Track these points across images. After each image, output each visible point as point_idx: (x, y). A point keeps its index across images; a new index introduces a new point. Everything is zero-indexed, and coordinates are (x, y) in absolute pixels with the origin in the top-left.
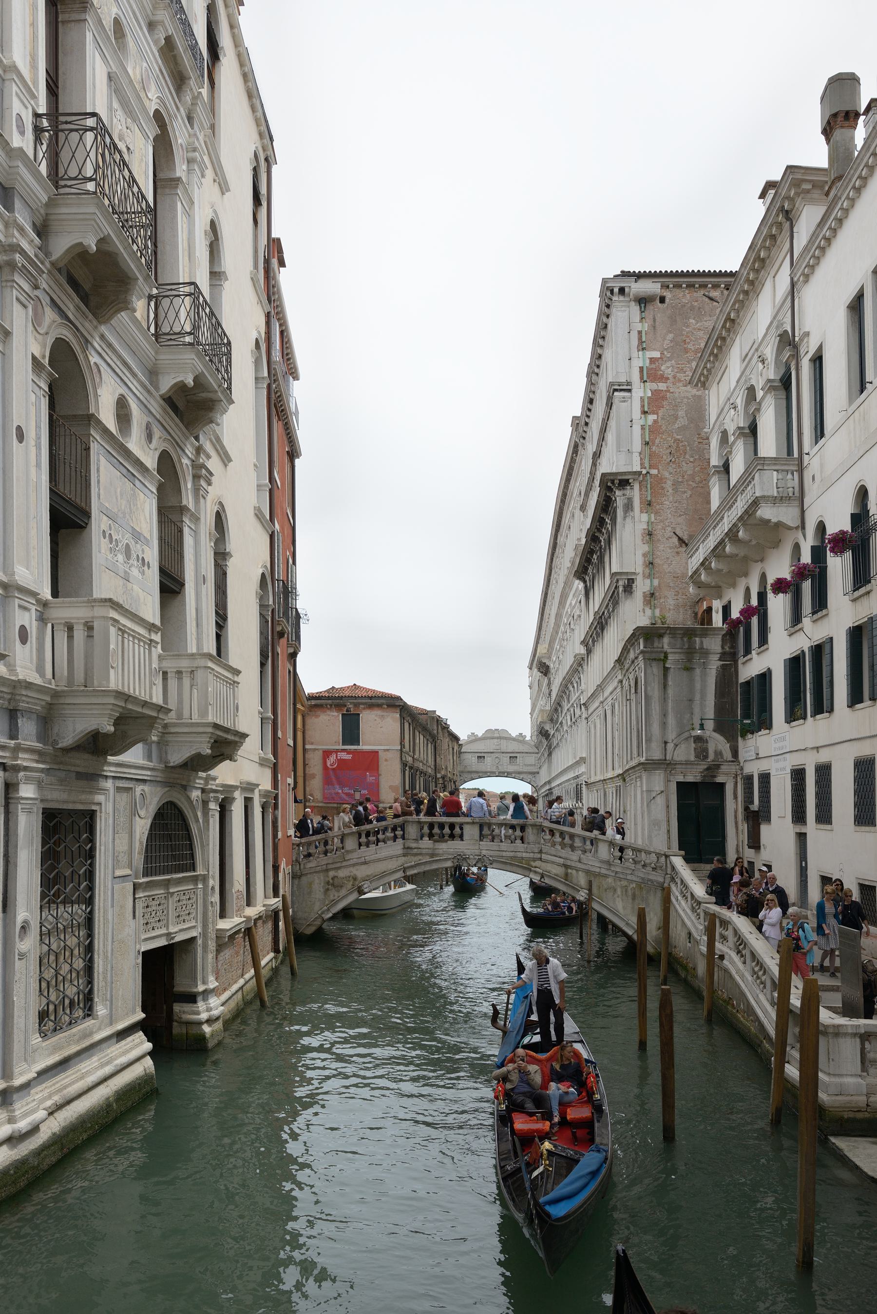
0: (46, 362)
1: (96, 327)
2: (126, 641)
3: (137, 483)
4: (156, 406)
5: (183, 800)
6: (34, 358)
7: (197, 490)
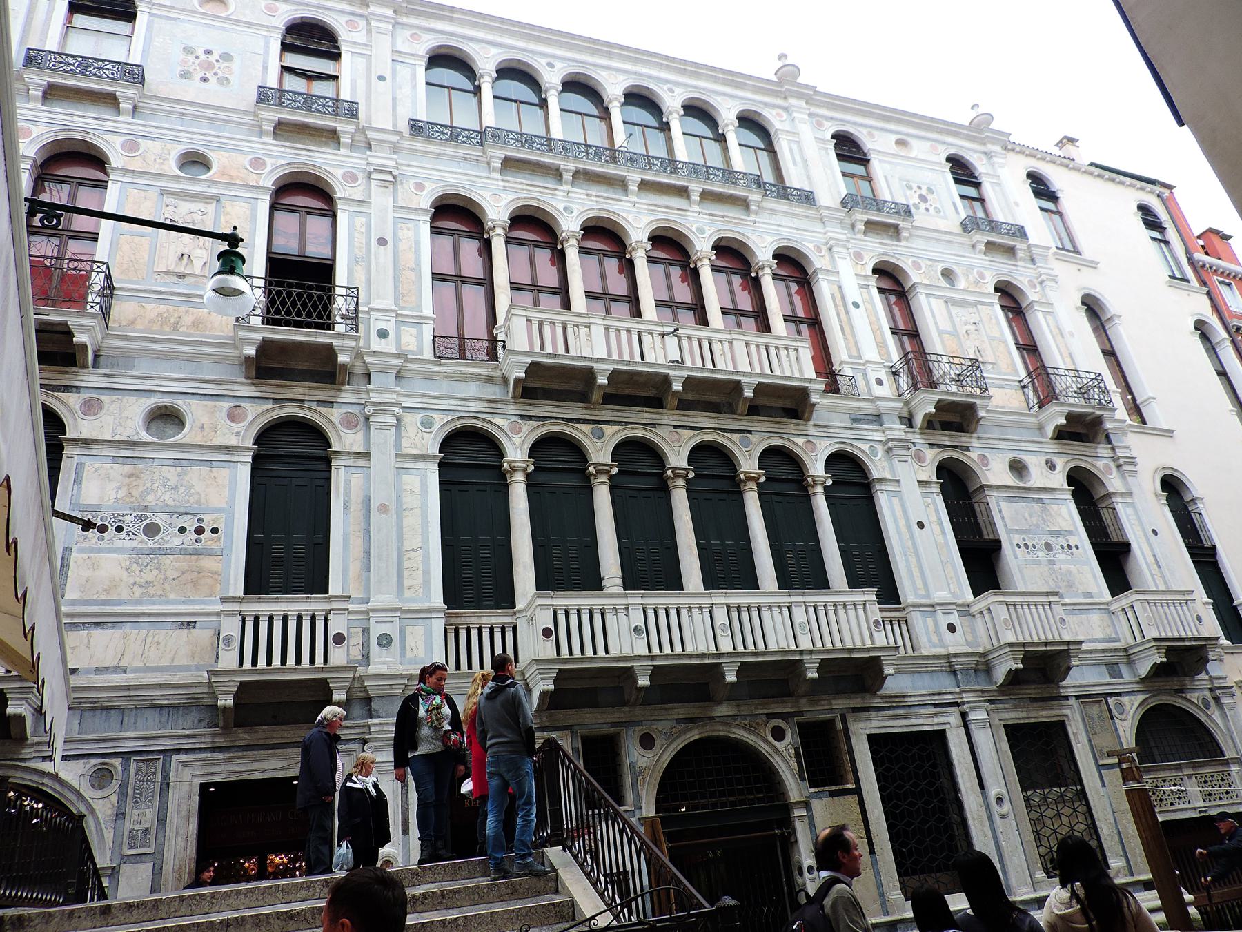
0: (935, 479)
4: (1052, 447)
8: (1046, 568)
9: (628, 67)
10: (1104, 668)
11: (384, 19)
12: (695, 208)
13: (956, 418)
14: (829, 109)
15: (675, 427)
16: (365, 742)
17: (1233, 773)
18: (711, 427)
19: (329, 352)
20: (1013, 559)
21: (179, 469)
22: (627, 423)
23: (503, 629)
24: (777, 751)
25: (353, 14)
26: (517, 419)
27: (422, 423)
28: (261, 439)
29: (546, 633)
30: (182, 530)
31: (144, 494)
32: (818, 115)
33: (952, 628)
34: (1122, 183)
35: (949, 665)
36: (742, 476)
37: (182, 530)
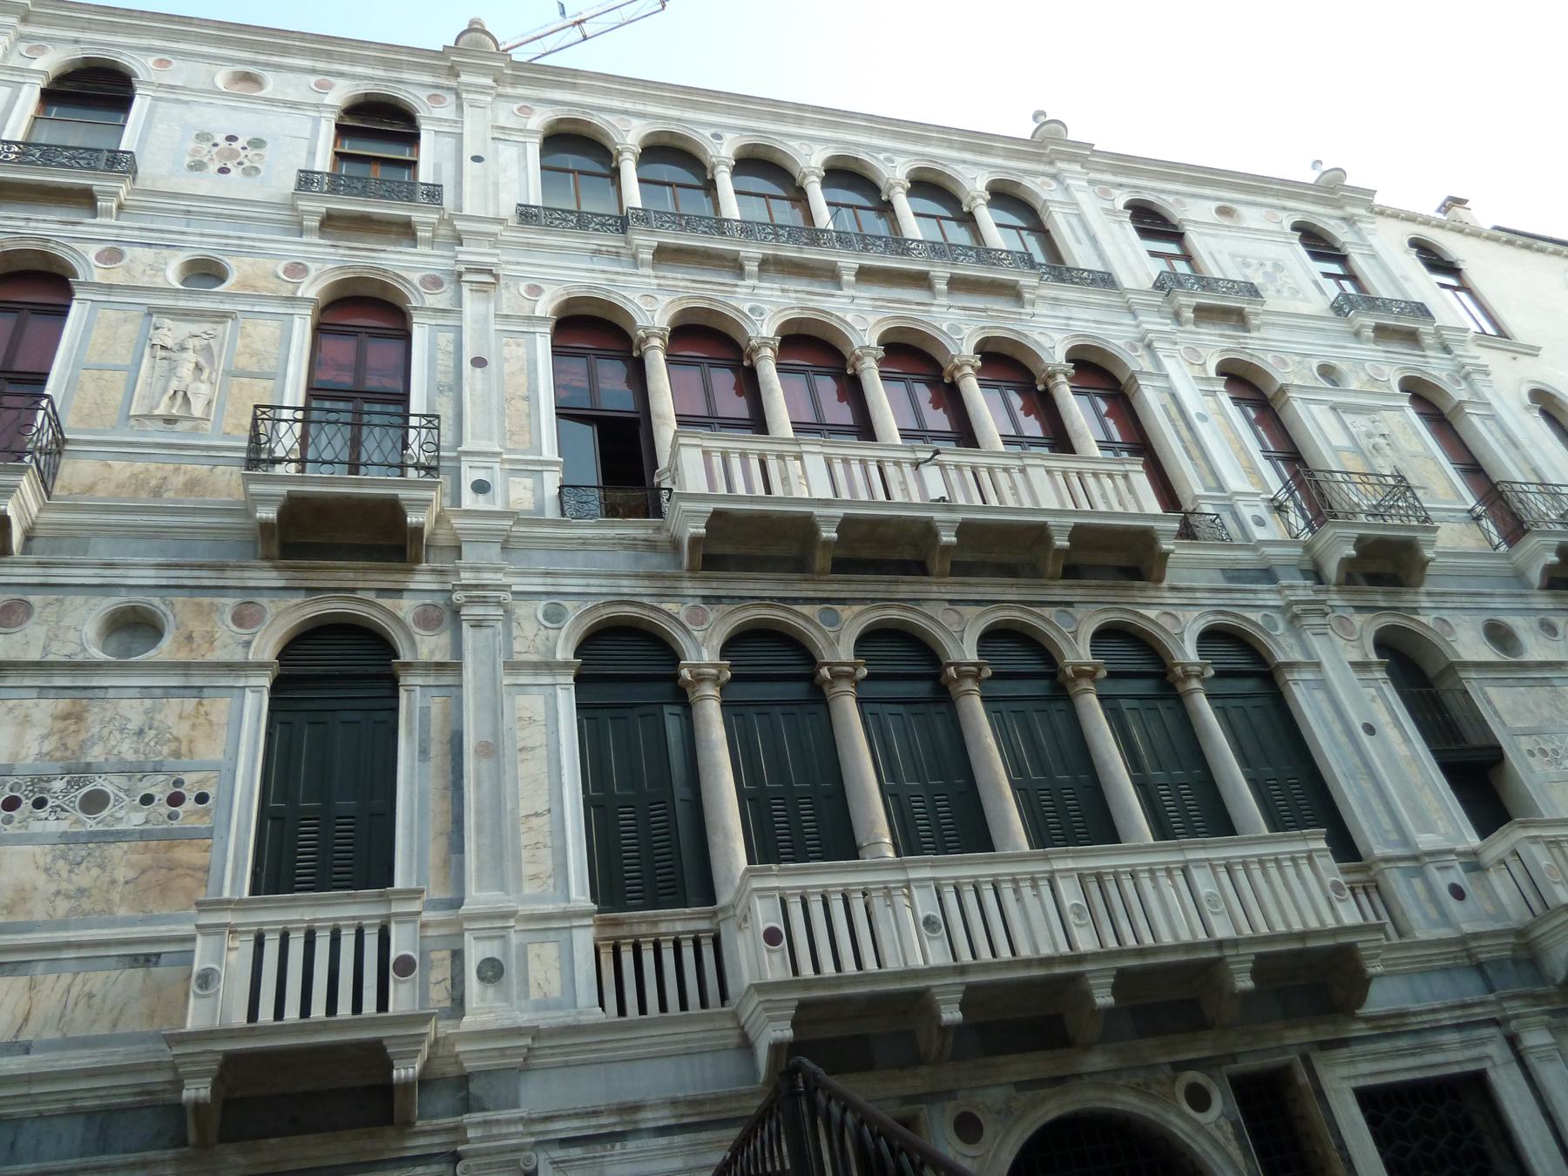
0: (1374, 657)
3: (1556, 682)
4: (1542, 601)
9: (826, 134)
11: (483, 90)
14: (1115, 174)
15: (951, 601)
16: (456, 1158)
18: (1006, 601)
19: (392, 510)
20: (1529, 768)
21: (148, 702)
22: (873, 600)
24: (1200, 1128)
25: (437, 87)
26: (698, 601)
27: (546, 616)
28: (285, 654)
29: (772, 937)
30: (147, 800)
31: (82, 745)
32: (1101, 182)
33: (1458, 893)
34: (1541, 250)
35: (1466, 956)
36: (1069, 671)
37: (147, 800)
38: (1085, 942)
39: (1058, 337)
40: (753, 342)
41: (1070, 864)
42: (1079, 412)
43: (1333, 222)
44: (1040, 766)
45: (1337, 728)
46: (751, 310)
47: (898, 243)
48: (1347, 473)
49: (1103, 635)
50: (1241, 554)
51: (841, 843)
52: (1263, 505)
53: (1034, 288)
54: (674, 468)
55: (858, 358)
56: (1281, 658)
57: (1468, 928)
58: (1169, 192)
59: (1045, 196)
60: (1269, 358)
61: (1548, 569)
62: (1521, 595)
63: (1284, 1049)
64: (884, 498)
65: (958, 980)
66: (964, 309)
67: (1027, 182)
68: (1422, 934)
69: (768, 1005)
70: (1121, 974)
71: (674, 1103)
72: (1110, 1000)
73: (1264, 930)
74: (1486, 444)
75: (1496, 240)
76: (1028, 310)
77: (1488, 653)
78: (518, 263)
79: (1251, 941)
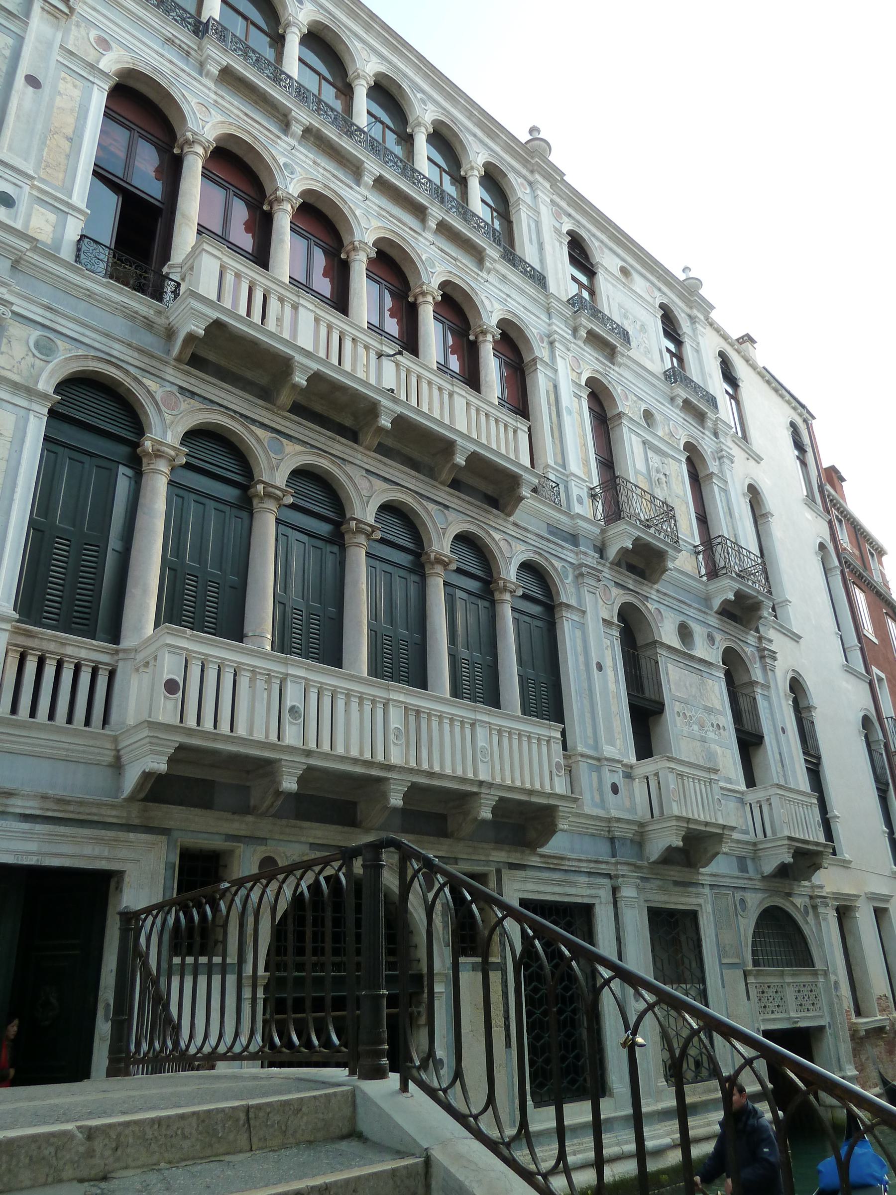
0: (615, 620)
1: (651, 587)
2: (686, 782)
3: (704, 674)
4: (714, 621)
5: (788, 904)
6: (604, 620)
7: (764, 668)
8: (699, 744)
10: (735, 859)
12: (430, 236)
13: (644, 562)
14: (569, 205)
15: (367, 471)
17: (820, 985)
22: (312, 446)
23: (60, 665)
26: (175, 389)
27: (37, 345)
29: (171, 686)
34: (782, 396)
36: (432, 556)
38: (396, 758)
39: (497, 306)
40: (279, 193)
41: (402, 698)
42: (491, 368)
43: (683, 315)
44: (391, 620)
45: (581, 659)
46: (285, 164)
47: (408, 169)
48: (654, 497)
49: (300, 474)
50: (564, 519)
51: (234, 628)
52: (586, 490)
53: (495, 261)
54: (190, 266)
55: (355, 249)
56: (564, 599)
57: (614, 813)
58: (597, 238)
59: (520, 194)
60: (619, 389)
61: (726, 602)
62: (705, 613)
63: (488, 863)
64: (324, 357)
65: (303, 760)
66: (442, 250)
67: (511, 176)
68: (588, 810)
69: (154, 740)
70: (414, 787)
71: (44, 797)
72: (489, 816)
73: (508, 782)
74: (716, 507)
75: (763, 377)
76: (484, 275)
77: (676, 643)
78: (94, 9)
79: (501, 787)
